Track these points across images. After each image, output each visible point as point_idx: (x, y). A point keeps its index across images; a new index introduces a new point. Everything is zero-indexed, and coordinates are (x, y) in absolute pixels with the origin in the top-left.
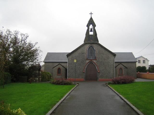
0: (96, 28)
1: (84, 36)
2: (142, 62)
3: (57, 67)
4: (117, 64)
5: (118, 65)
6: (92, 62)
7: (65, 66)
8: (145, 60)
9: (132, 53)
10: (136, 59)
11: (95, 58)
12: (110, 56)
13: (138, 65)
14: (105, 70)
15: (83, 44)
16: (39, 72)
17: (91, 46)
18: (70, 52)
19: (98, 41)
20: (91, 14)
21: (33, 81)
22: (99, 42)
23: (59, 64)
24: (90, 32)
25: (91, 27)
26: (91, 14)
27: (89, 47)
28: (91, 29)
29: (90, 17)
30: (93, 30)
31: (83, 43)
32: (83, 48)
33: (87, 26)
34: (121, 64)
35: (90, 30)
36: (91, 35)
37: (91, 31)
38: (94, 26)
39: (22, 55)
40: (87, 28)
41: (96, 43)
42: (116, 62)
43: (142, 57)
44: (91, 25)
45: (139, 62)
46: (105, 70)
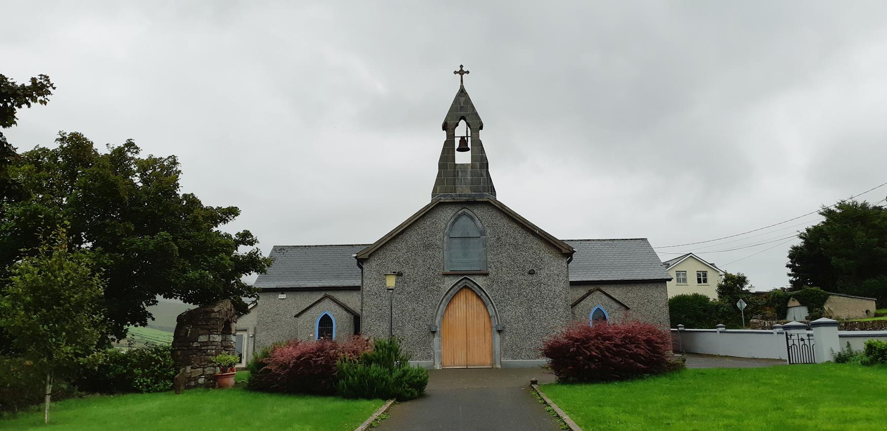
0: (483, 135)
1: (435, 171)
2: (692, 278)
3: (317, 314)
4: (582, 291)
5: (588, 295)
6: (470, 284)
7: (351, 306)
8: (704, 269)
9: (645, 240)
10: (667, 265)
11: (229, 354)
12: (547, 255)
13: (674, 290)
14: (526, 321)
15: (428, 206)
16: (223, 340)
17: (466, 287)
18: (371, 236)
19: (495, 195)
20: (461, 72)
21: (193, 383)
22: (499, 198)
23: (325, 297)
24: (457, 153)
25: (461, 130)
26: (461, 72)
27: (455, 216)
28: (463, 141)
29: (458, 88)
30: (469, 146)
31: (426, 199)
32: (428, 222)
33: (443, 130)
34: (598, 290)
35: (457, 145)
36: (463, 166)
37: (463, 148)
38: (476, 125)
39: (78, 260)
40: (443, 136)
41: (487, 203)
42: (573, 284)
43: (691, 256)
44: (462, 123)
45: (682, 278)
46: (526, 321)
